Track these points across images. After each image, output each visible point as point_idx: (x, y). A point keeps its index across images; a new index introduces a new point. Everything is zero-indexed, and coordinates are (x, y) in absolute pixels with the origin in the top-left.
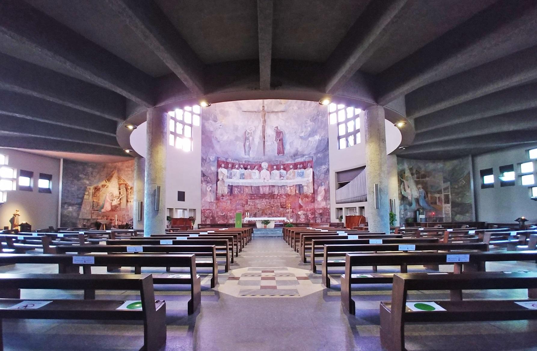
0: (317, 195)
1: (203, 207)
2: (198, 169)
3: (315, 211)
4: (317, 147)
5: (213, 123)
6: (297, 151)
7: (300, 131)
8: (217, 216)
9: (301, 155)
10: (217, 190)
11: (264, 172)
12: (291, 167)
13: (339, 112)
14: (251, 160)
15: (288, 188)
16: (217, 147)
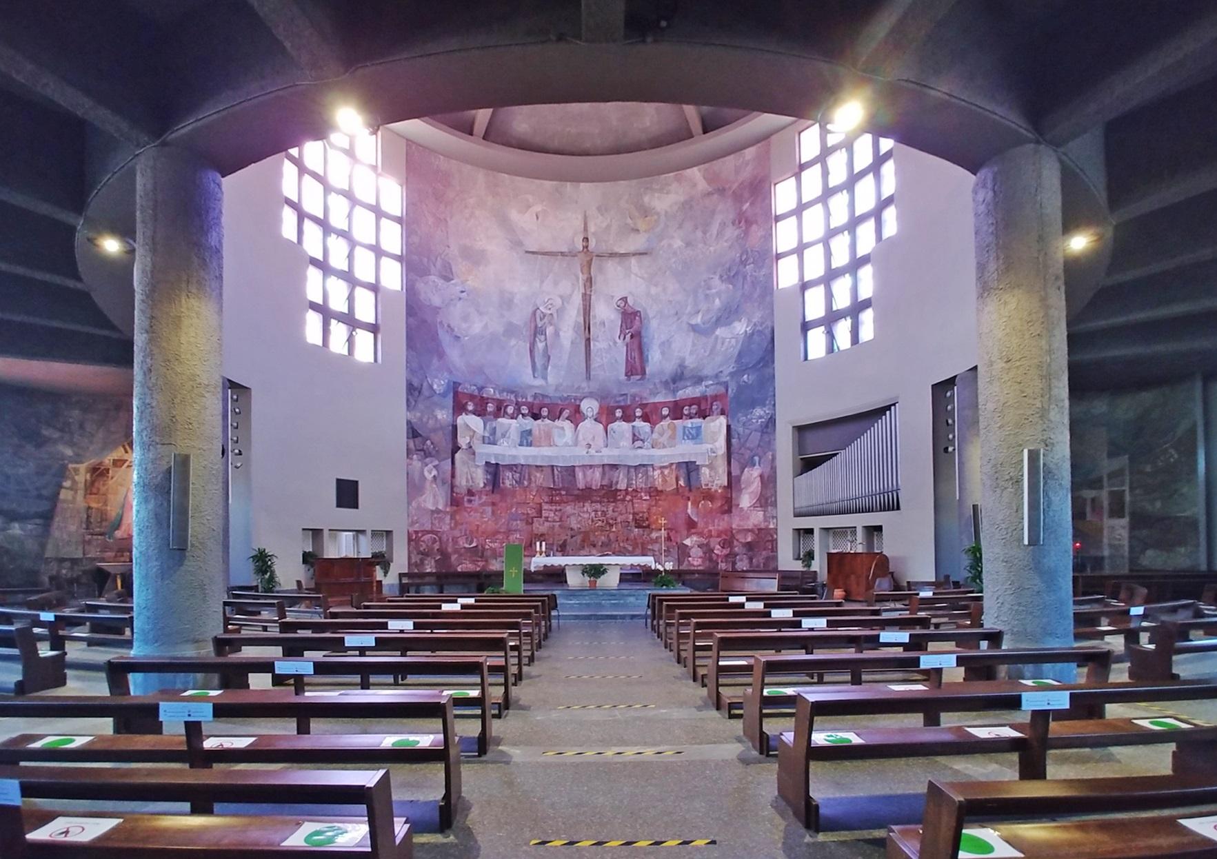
0: (740, 490)
1: (413, 524)
2: (397, 415)
3: (733, 536)
4: (740, 355)
5: (440, 282)
6: (682, 366)
8: (456, 551)
9: (693, 377)
10: (453, 476)
12: (665, 411)
14: (551, 392)
15: (657, 473)
16: (454, 354)
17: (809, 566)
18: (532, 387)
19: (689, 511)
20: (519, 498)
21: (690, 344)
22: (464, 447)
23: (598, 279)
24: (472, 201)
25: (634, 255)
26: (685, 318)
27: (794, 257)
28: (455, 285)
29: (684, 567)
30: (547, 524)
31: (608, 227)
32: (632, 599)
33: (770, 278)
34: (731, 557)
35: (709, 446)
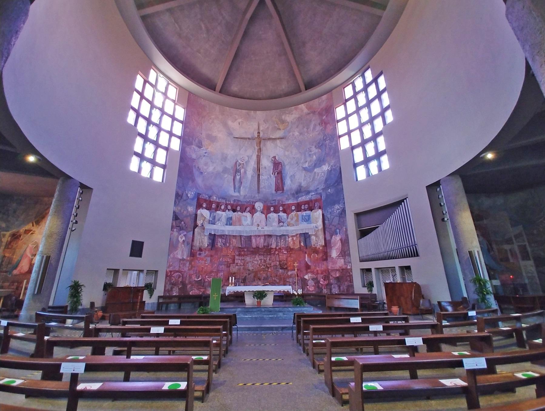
0: (331, 248)
1: (169, 266)
2: (170, 208)
3: (329, 273)
4: (326, 180)
5: (196, 148)
6: (300, 186)
7: (302, 161)
8: (190, 283)
9: (305, 191)
10: (193, 240)
12: (293, 208)
14: (241, 199)
15: (290, 239)
16: (199, 180)
17: (371, 291)
18: (232, 196)
19: (306, 259)
20: (224, 253)
21: (303, 175)
22: (200, 225)
23: (264, 149)
24: (213, 117)
25: (278, 139)
26: (300, 165)
27: (347, 137)
28: (203, 150)
29: (305, 292)
30: (237, 267)
31: (268, 128)
32: (281, 314)
33: (337, 145)
34: (329, 285)
35: (315, 225)
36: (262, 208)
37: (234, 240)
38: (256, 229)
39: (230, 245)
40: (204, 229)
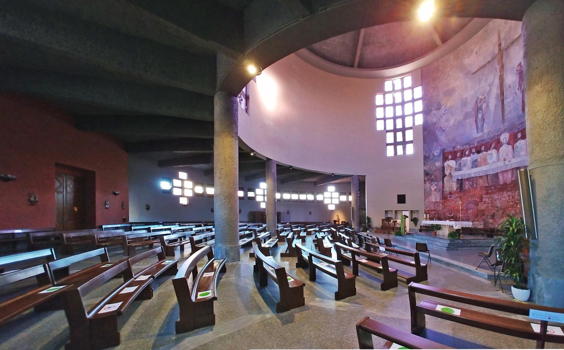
1: (426, 208)
10: (443, 187)
11: (505, 149)
13: (406, 105)
14: (485, 137)
16: (443, 138)
18: (475, 138)
30: (485, 205)
36: (508, 139)
37: (480, 181)
38: (502, 164)
39: (477, 186)
40: (452, 176)
